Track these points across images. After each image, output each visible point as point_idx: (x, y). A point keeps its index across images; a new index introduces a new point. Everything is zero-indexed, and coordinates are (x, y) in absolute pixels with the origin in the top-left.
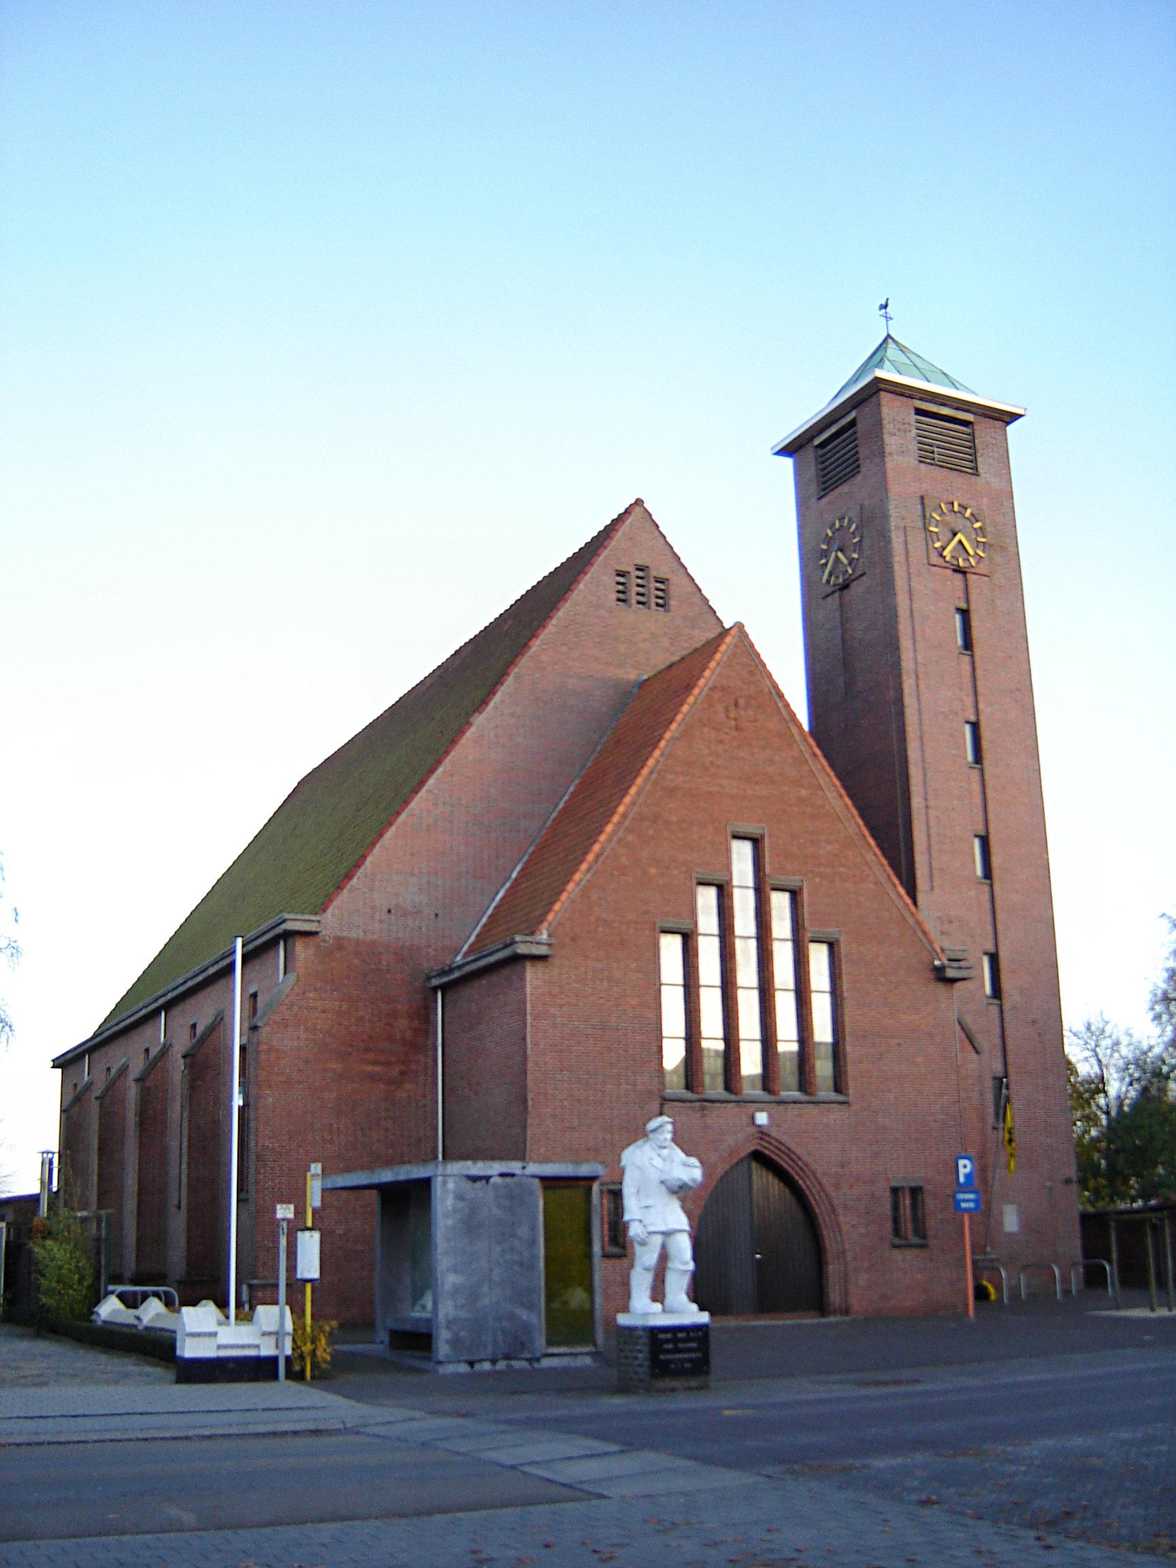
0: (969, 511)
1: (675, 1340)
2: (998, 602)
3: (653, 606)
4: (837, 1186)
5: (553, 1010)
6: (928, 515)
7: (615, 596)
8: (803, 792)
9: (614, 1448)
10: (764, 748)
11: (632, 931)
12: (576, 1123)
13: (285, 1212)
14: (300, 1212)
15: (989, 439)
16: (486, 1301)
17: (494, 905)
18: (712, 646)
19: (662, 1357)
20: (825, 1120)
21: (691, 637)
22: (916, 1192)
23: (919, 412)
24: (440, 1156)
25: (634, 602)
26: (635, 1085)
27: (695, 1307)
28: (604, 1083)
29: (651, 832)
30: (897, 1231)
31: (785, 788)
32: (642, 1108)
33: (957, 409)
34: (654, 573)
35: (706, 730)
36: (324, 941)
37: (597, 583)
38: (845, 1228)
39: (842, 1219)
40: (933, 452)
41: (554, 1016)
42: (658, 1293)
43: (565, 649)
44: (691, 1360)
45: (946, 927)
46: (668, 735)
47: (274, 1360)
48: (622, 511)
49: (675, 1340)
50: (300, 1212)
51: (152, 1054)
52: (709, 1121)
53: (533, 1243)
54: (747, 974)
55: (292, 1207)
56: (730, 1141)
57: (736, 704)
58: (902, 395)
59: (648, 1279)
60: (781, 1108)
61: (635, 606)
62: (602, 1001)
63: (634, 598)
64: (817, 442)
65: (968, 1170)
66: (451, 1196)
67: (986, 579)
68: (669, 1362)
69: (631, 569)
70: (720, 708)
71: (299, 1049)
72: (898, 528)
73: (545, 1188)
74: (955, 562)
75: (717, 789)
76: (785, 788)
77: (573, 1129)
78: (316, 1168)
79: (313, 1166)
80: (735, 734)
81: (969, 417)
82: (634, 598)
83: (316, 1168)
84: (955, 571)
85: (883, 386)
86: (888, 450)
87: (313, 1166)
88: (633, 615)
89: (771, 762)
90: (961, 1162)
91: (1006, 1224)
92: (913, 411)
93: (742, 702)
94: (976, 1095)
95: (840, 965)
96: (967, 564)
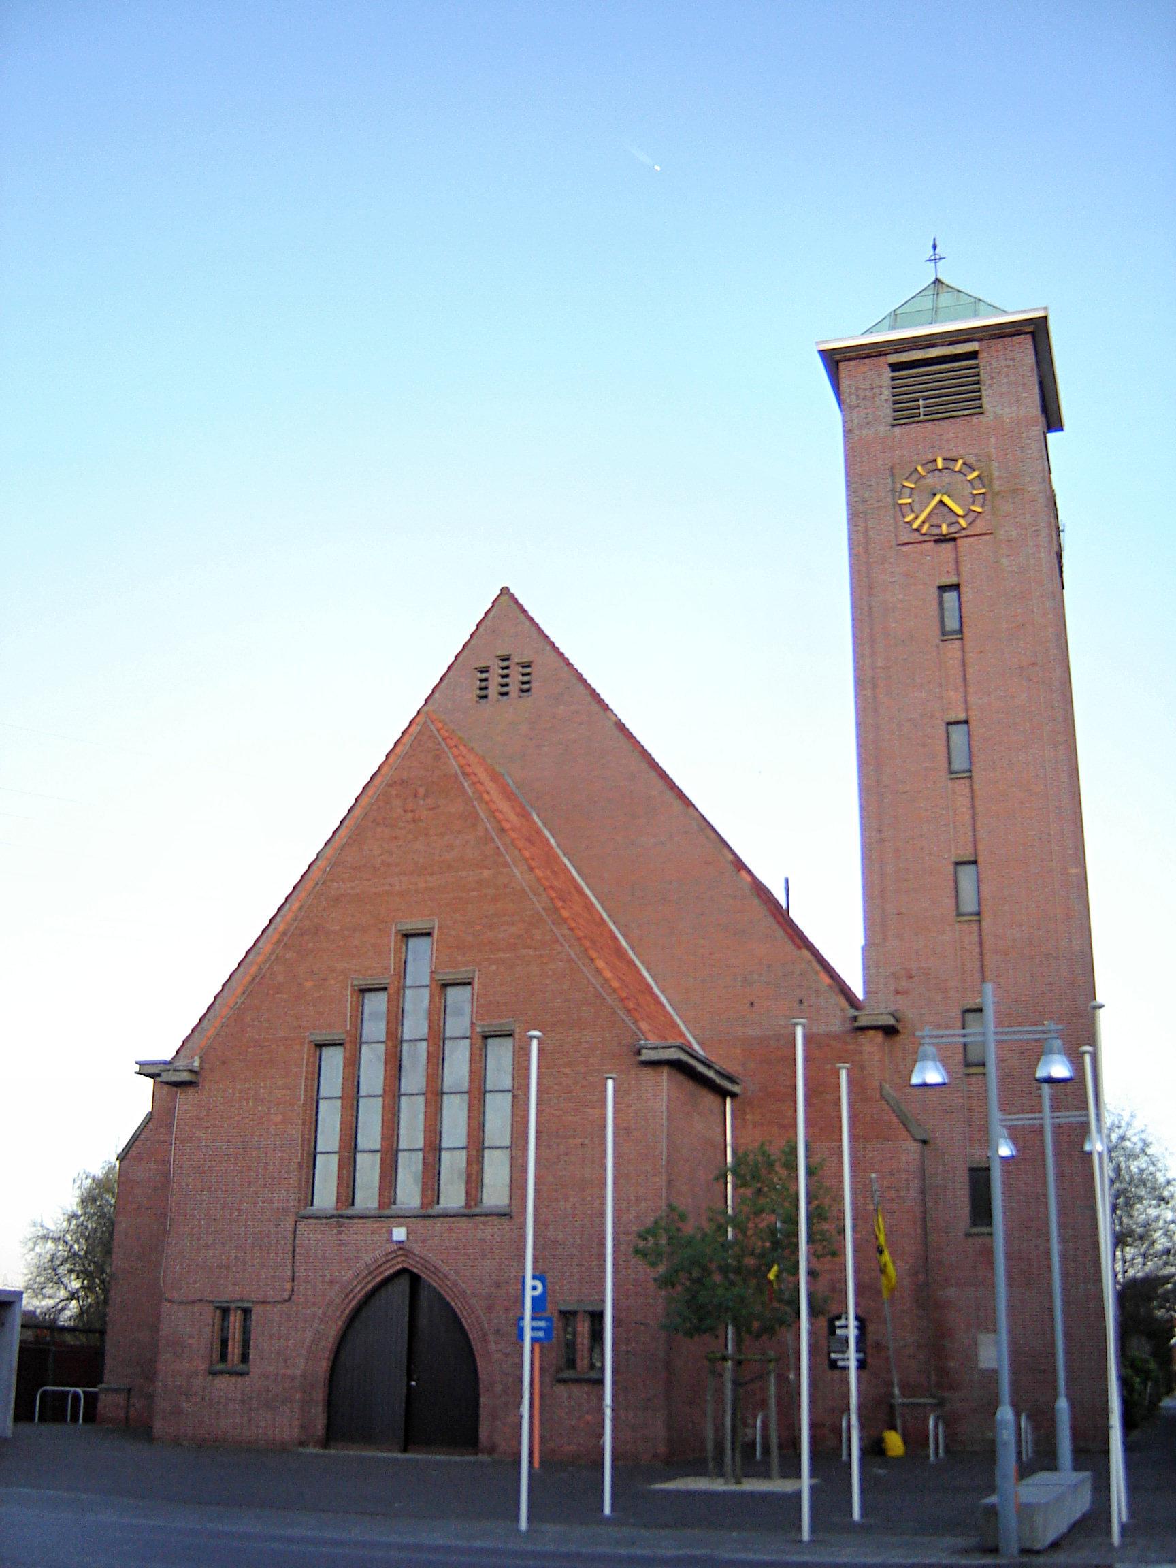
0: (940, 461)
2: (1005, 561)
4: (490, 1308)
5: (198, 1133)
8: (486, 873)
10: (442, 835)
11: (282, 1048)
12: (210, 1241)
15: (1003, 363)
20: (480, 1235)
23: (895, 367)
26: (271, 1202)
28: (241, 1202)
29: (310, 945)
31: (464, 874)
32: (277, 1226)
33: (951, 344)
35: (379, 830)
38: (497, 1356)
39: (493, 1346)
41: (199, 1139)
45: (904, 984)
52: (344, 1237)
56: (367, 1258)
58: (868, 356)
60: (429, 1222)
62: (247, 1121)
67: (987, 537)
70: (397, 803)
71: (150, 1178)
75: (387, 888)
76: (464, 874)
77: (207, 1247)
80: (412, 826)
81: (973, 346)
84: (936, 541)
85: (838, 357)
89: (450, 847)
91: (981, 1358)
92: (889, 369)
93: (422, 791)
94: (913, 1194)
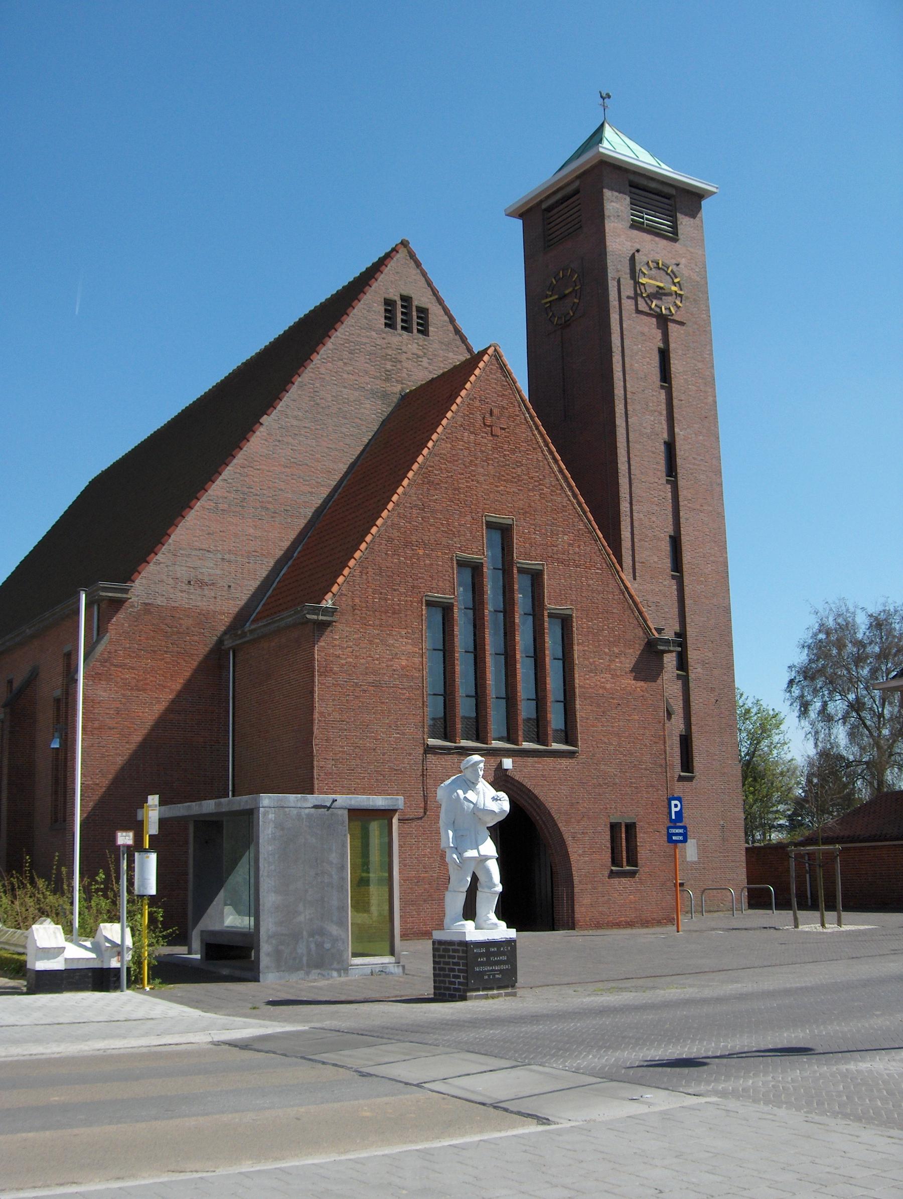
1: (488, 954)
3: (415, 331)
6: (637, 269)
7: (383, 321)
9: (508, 1063)
13: (125, 838)
14: (139, 838)
16: (301, 918)
17: (278, 580)
18: (475, 359)
19: (477, 969)
21: (446, 358)
22: (631, 828)
24: (230, 793)
25: (399, 327)
27: (503, 924)
30: (615, 861)
34: (415, 303)
36: (133, 606)
37: (368, 310)
40: (642, 218)
42: (470, 912)
43: (340, 363)
44: (501, 971)
46: (435, 437)
47: (117, 971)
48: (382, 255)
49: (488, 954)
50: (139, 838)
51: (16, 685)
53: (343, 868)
54: (492, 642)
55: (131, 834)
57: (491, 414)
59: (461, 899)
61: (399, 331)
63: (399, 324)
64: (544, 206)
65: (678, 809)
66: (272, 825)
68: (482, 973)
69: (397, 299)
72: (614, 279)
73: (350, 819)
74: (658, 310)
78: (153, 800)
79: (150, 798)
82: (399, 324)
83: (153, 800)
86: (607, 213)
87: (150, 798)
88: (398, 338)
90: (673, 803)
92: (627, 183)
95: (453, 665)
96: (668, 313)
